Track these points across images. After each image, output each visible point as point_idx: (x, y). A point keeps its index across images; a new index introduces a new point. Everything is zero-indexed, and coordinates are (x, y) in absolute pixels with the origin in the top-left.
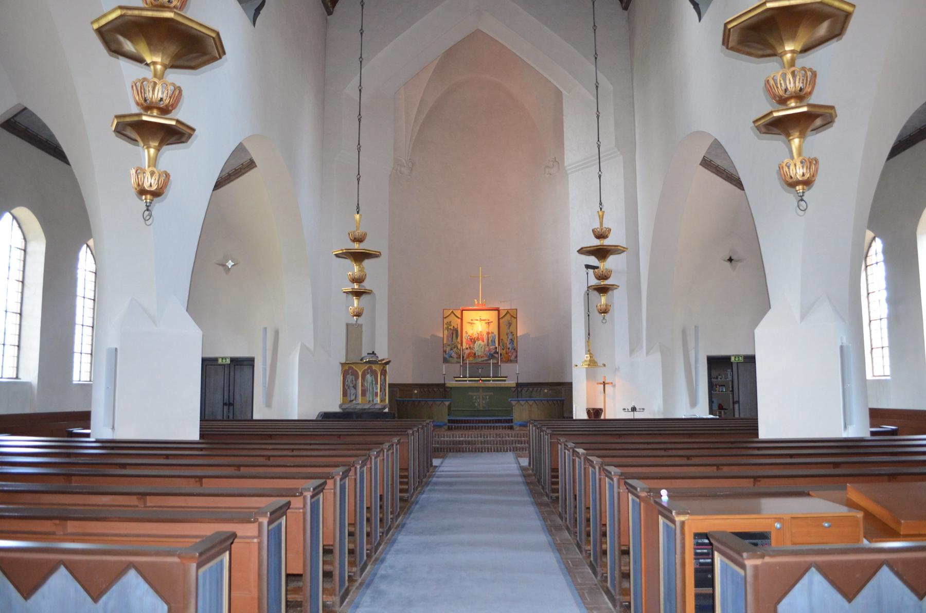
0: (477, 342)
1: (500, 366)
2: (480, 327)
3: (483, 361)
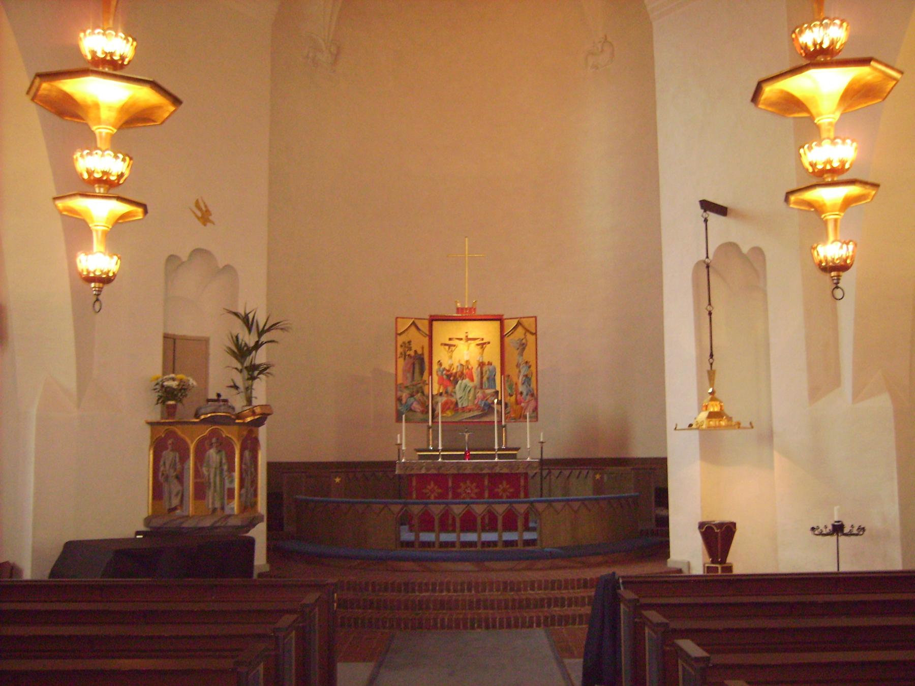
0: (460, 382)
1: (505, 426)
2: (465, 352)
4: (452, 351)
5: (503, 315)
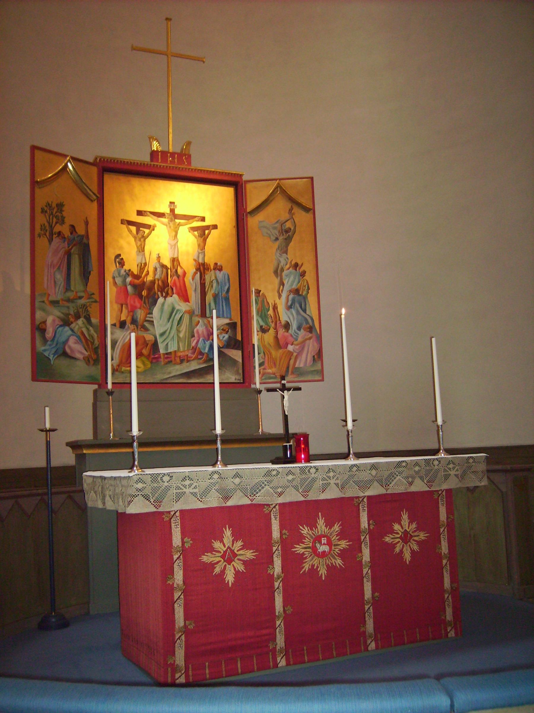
0: (161, 300)
3: (188, 375)
4: (144, 238)
5: (241, 176)
